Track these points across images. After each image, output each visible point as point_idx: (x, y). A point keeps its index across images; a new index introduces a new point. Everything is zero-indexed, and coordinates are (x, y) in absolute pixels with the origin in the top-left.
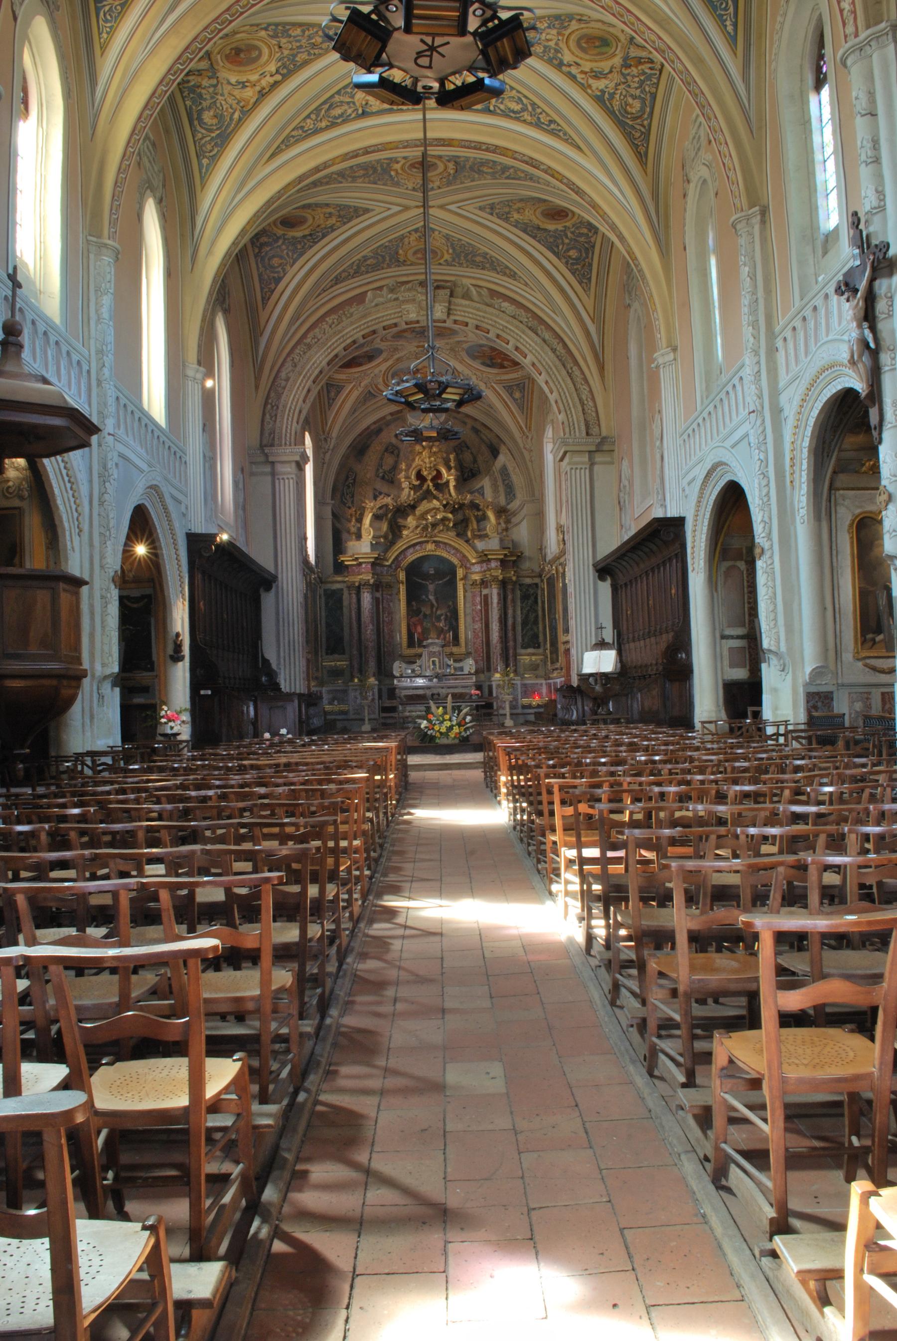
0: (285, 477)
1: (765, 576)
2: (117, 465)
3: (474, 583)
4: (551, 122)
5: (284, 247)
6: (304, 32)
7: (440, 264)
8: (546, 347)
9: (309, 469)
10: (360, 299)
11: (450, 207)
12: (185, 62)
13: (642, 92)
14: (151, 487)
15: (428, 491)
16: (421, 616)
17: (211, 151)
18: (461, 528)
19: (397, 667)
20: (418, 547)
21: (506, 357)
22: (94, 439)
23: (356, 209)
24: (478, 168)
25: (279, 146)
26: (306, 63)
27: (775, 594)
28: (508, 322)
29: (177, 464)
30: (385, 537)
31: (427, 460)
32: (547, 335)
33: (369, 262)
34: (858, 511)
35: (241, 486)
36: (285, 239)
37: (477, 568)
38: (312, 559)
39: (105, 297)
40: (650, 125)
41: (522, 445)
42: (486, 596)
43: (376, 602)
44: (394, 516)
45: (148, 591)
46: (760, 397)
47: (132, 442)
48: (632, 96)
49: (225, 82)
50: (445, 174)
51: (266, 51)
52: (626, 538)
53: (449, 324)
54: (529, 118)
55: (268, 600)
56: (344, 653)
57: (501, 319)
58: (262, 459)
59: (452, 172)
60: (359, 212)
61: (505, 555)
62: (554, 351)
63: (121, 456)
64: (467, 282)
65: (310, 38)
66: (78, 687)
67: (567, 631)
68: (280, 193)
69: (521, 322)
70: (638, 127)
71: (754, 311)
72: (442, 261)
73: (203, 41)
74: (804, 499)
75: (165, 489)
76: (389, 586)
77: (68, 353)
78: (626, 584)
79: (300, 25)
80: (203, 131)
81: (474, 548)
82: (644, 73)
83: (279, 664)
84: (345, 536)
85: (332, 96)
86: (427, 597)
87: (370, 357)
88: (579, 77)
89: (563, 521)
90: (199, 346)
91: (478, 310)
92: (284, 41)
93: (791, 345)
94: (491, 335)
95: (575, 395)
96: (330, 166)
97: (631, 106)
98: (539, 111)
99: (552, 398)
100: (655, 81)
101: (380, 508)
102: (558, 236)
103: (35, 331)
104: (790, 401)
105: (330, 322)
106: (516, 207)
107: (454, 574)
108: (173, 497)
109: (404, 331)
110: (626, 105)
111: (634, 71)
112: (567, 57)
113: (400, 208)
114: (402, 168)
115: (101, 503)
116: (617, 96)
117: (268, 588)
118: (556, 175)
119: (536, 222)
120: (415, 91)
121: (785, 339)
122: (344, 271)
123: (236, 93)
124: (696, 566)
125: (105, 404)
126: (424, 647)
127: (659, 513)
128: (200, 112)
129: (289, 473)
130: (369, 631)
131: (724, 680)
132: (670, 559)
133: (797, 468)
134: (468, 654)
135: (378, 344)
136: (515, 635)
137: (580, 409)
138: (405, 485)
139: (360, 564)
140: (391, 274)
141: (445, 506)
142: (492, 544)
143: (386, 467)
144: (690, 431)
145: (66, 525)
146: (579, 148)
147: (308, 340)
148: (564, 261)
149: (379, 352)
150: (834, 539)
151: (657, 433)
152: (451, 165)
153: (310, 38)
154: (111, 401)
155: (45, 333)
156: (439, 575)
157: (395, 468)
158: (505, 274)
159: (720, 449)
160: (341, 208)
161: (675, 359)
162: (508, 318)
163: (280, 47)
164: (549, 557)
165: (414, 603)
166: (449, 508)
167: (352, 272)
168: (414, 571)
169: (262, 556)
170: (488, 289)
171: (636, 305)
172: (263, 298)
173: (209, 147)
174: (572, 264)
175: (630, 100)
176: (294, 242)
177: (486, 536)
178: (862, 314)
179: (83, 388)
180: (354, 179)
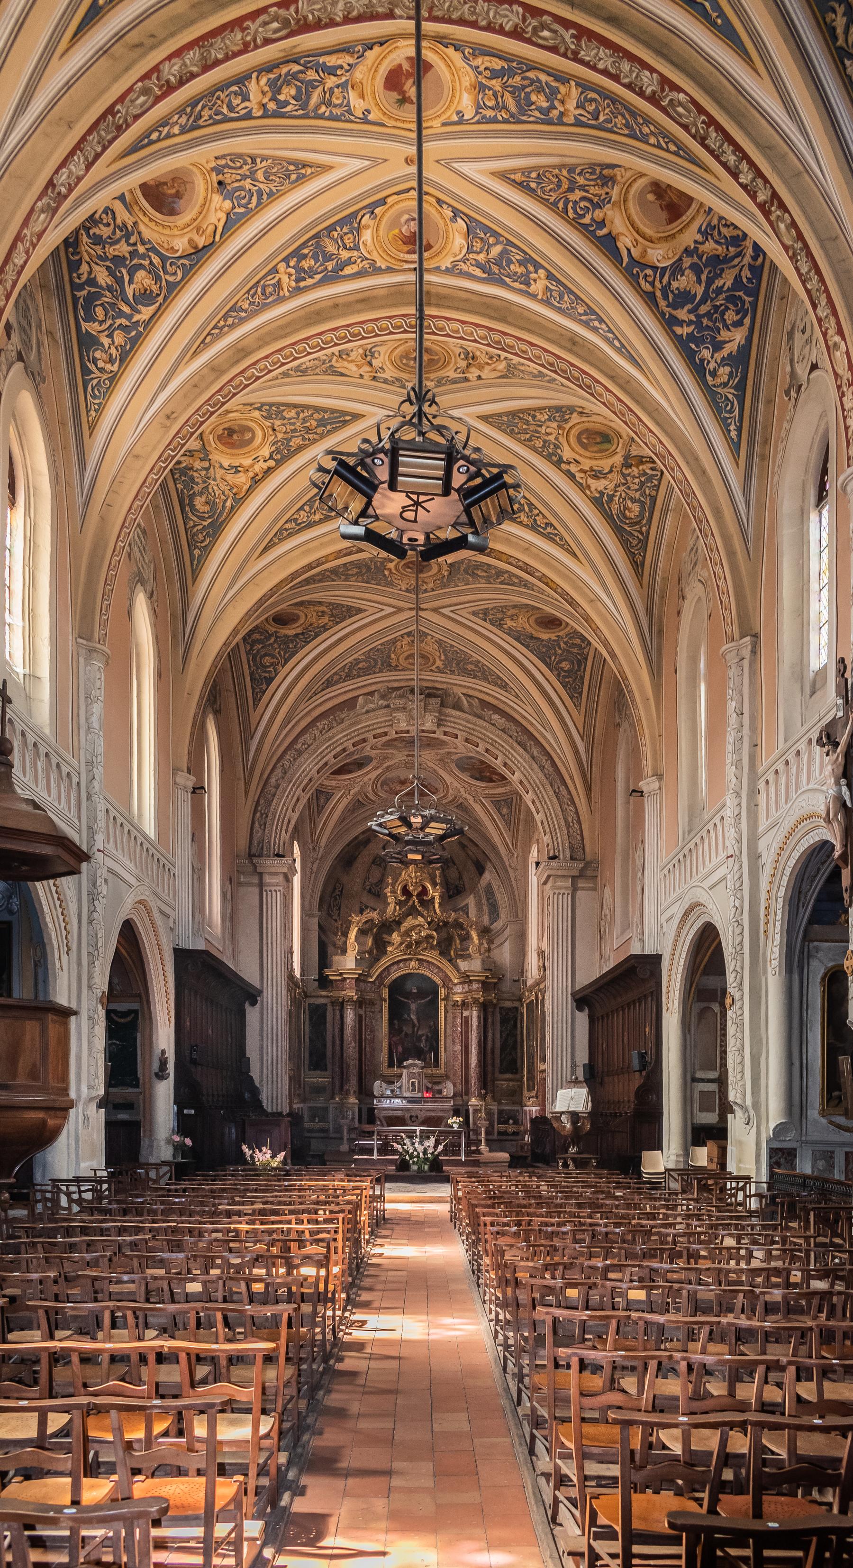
0: (273, 889)
1: (734, 1026)
2: (106, 880)
3: (455, 1004)
4: (547, 524)
5: (276, 645)
6: (298, 414)
7: (432, 671)
8: (534, 764)
9: (297, 880)
10: (351, 704)
11: (443, 611)
12: (175, 448)
13: (641, 495)
14: (139, 902)
15: (413, 906)
16: (403, 1035)
17: (203, 541)
18: (444, 948)
19: (378, 1086)
20: (401, 965)
21: (494, 771)
22: (84, 866)
23: (349, 608)
25: (271, 540)
26: (300, 449)
27: (743, 1046)
28: (497, 736)
30: (370, 952)
31: (413, 875)
32: (536, 752)
33: (360, 665)
34: (831, 964)
35: (229, 896)
36: (277, 637)
37: (459, 989)
38: (297, 974)
39: (95, 705)
40: (648, 531)
41: (507, 863)
42: (466, 1018)
43: (360, 1019)
45: (135, 1006)
46: (739, 841)
47: (121, 857)
48: (631, 499)
49: (217, 465)
50: (439, 576)
51: (259, 434)
52: (605, 971)
53: (439, 735)
54: (526, 519)
55: (252, 1014)
56: (326, 1070)
57: (491, 732)
58: (251, 869)
59: (446, 574)
60: (351, 612)
61: (487, 977)
62: (542, 768)
63: (111, 871)
64: (458, 691)
65: (304, 420)
66: (65, 1118)
67: (543, 1060)
68: (272, 592)
70: (636, 534)
71: (738, 751)
72: (433, 668)
73: (194, 425)
74: (777, 950)
75: (153, 904)
76: (372, 1003)
77: (58, 765)
78: (602, 1017)
79: (295, 406)
80: (195, 519)
81: (458, 969)
82: (645, 474)
83: (262, 1081)
84: (330, 949)
86: (409, 1015)
87: (360, 764)
88: (578, 476)
89: (544, 947)
90: (189, 753)
91: (468, 721)
92: (277, 423)
93: (772, 789)
94: (481, 749)
95: (561, 816)
96: (323, 564)
97: (630, 510)
98: (536, 512)
99: (538, 818)
100: (656, 482)
101: (366, 922)
102: (552, 645)
103: (25, 743)
104: (768, 847)
105: (321, 727)
106: (509, 613)
107: (436, 993)
108: (162, 912)
109: (395, 740)
110: (625, 508)
111: (635, 471)
112: (567, 453)
113: (392, 610)
114: (396, 567)
115: (90, 922)
116: (616, 499)
117: (254, 1003)
118: (551, 584)
120: (401, 542)
121: (767, 782)
122: (335, 673)
123: (229, 477)
124: (670, 1005)
125: (95, 819)
126: (404, 1067)
127: (636, 949)
128: (192, 497)
129: (277, 885)
130: (351, 1048)
131: (693, 1124)
132: (645, 997)
133: (771, 918)
134: (447, 1077)
135: (368, 751)
136: (493, 1059)
137: (566, 831)
138: (391, 900)
139: (345, 979)
140: (383, 679)
141: (429, 923)
142: (473, 965)
143: (374, 879)
144: (670, 866)
145: (55, 943)
146: (574, 555)
147: (298, 746)
148: (556, 673)
149: (369, 759)
150: (805, 992)
151: (639, 864)
153: (304, 420)
154: (101, 815)
155: (35, 745)
156: (421, 994)
157: (381, 881)
158: (496, 685)
159: (699, 889)
160: (334, 606)
161: (660, 789)
162: (497, 731)
163: (274, 430)
164: (530, 983)
165: (396, 1022)
166: (433, 925)
167: (343, 674)
168: (397, 988)
169: (249, 971)
171: (625, 725)
172: (254, 699)
173: (201, 537)
174: (564, 677)
175: (629, 504)
176: (287, 640)
178: (841, 769)
179: (73, 802)
180: (347, 577)
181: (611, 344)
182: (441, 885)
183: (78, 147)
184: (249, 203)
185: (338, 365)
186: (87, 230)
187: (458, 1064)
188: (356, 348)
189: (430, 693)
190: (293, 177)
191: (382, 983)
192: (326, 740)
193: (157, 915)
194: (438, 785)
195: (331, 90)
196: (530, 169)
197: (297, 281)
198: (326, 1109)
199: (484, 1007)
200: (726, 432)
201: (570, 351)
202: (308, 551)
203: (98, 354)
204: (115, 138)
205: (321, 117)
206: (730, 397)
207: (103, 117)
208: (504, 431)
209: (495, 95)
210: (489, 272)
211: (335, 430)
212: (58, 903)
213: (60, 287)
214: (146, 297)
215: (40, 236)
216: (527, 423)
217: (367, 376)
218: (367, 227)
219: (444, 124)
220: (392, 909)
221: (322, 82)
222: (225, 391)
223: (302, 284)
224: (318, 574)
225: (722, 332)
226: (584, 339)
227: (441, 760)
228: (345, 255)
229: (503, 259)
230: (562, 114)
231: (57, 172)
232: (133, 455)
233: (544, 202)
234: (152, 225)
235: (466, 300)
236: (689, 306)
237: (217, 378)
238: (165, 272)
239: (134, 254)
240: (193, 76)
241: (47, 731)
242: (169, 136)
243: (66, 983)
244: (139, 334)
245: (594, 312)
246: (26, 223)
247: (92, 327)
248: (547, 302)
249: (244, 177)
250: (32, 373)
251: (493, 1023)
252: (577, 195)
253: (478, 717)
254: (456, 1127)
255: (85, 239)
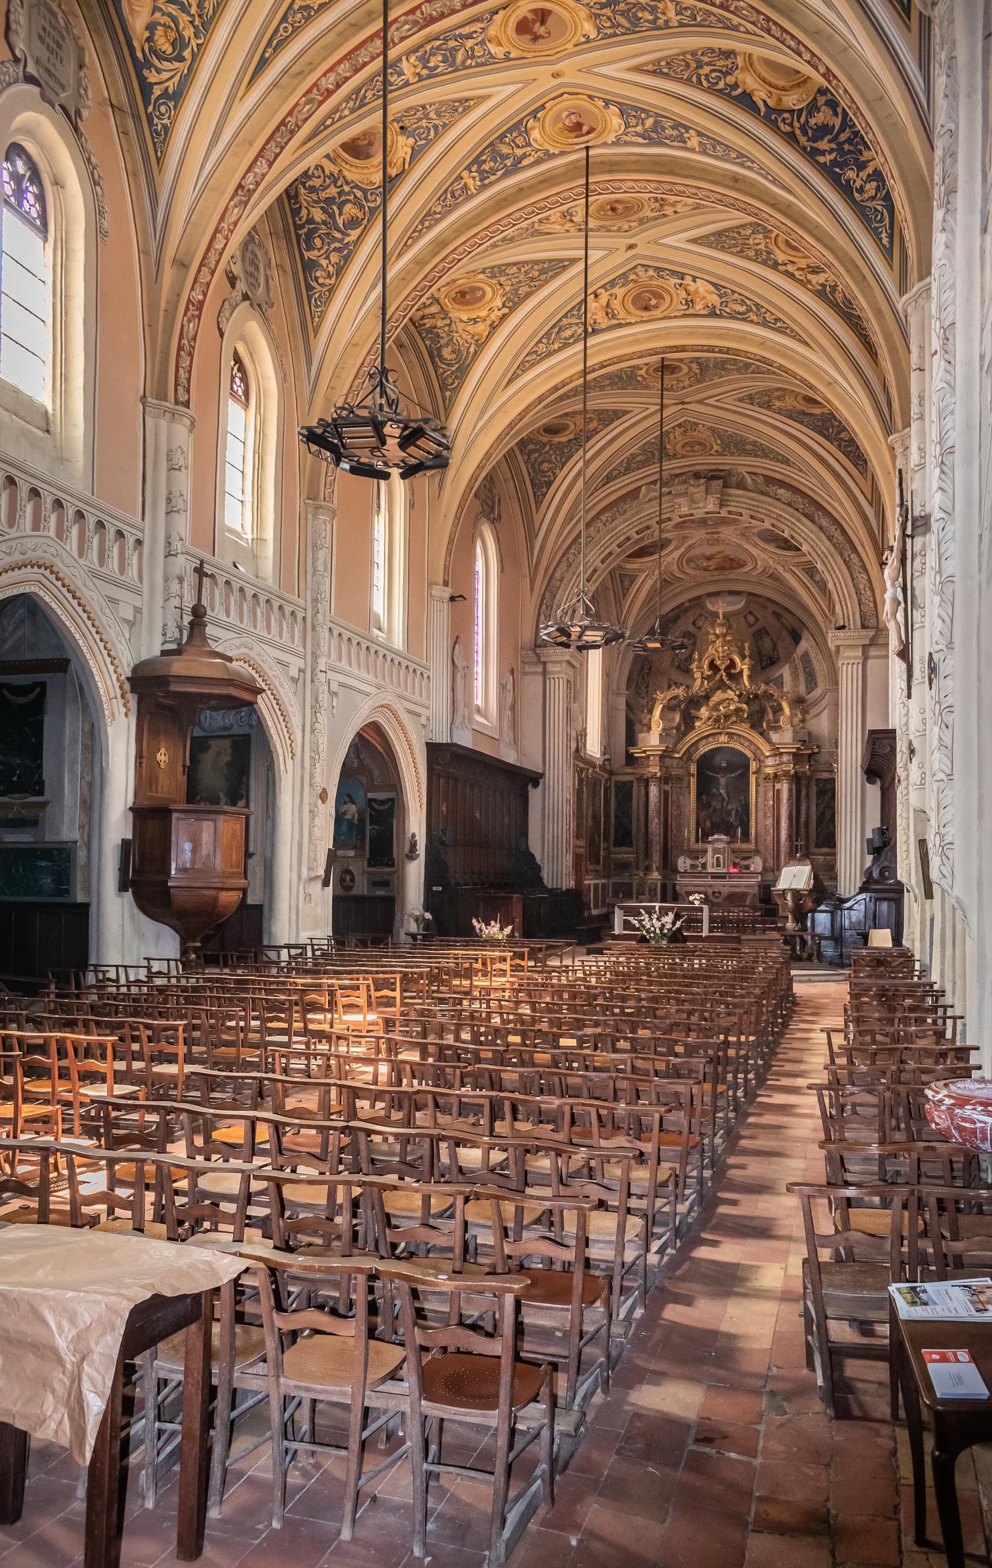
3: (767, 778)
15: (721, 680)
16: (711, 810)
20: (710, 739)
23: (615, 412)
24: (721, 366)
26: (528, 295)
28: (782, 510)
29: (417, 681)
30: (678, 728)
31: (720, 650)
32: (824, 522)
37: (770, 762)
42: (779, 791)
43: (665, 795)
44: (687, 707)
45: (391, 795)
55: (535, 795)
56: (631, 845)
58: (535, 659)
60: (617, 414)
61: (798, 749)
62: (830, 538)
64: (740, 469)
68: (521, 416)
69: (797, 510)
75: (399, 707)
76: (679, 779)
79: (514, 264)
81: (769, 741)
83: (543, 859)
84: (637, 727)
85: (560, 320)
88: (797, 274)
91: (752, 499)
92: (502, 279)
95: (851, 585)
98: (763, 310)
112: (781, 257)
114: (647, 372)
115: (313, 731)
117: (536, 785)
119: (799, 407)
122: (614, 469)
125: (318, 646)
129: (560, 672)
130: (655, 825)
134: (757, 852)
138: (697, 675)
141: (739, 696)
142: (785, 737)
146: (807, 344)
149: (669, 541)
152: (694, 366)
156: (731, 768)
157: (690, 659)
158: (778, 461)
162: (782, 506)
166: (744, 698)
167: (622, 470)
168: (706, 763)
170: (764, 476)
172: (536, 502)
173: (450, 380)
174: (846, 446)
177: (780, 728)
180: (602, 388)
181: (766, 178)
182: (750, 657)
183: (260, 155)
184: (428, 135)
185: (543, 228)
186: (304, 184)
187: (770, 838)
188: (555, 214)
189: (712, 476)
190: (460, 110)
191: (690, 759)
192: (609, 532)
193: (404, 716)
194: (744, 557)
195: (472, 49)
196: (659, 60)
197: (482, 180)
198: (631, 885)
199: (796, 779)
200: (877, 240)
201: (732, 188)
202: (552, 376)
203: (318, 274)
204: (289, 140)
205: (470, 67)
206: (879, 208)
207: (278, 129)
208: (716, 248)
209: (609, 18)
210: (650, 138)
211: (557, 274)
212: (281, 718)
213: (286, 231)
214: (353, 223)
215: (236, 224)
216: (735, 239)
217: (572, 230)
218: (533, 128)
219: (576, 45)
220: (698, 685)
221: (462, 45)
222: (430, 277)
223: (487, 182)
224: (570, 391)
225: (865, 153)
226: (744, 176)
227: (743, 535)
228: (519, 152)
229: (656, 127)
230: (667, 22)
231: (244, 177)
232: (353, 344)
233: (679, 80)
234: (353, 169)
235: (636, 162)
236: (829, 137)
237: (422, 268)
238: (367, 201)
239: (340, 194)
240: (347, 79)
241: (270, 581)
242: (341, 118)
243: (290, 782)
244: (350, 252)
245: (744, 156)
246: (222, 219)
247: (313, 254)
248: (704, 152)
249: (420, 119)
250: (259, 306)
251: (807, 796)
252: (707, 69)
253: (762, 493)
254: (697, 903)
255: (303, 191)
